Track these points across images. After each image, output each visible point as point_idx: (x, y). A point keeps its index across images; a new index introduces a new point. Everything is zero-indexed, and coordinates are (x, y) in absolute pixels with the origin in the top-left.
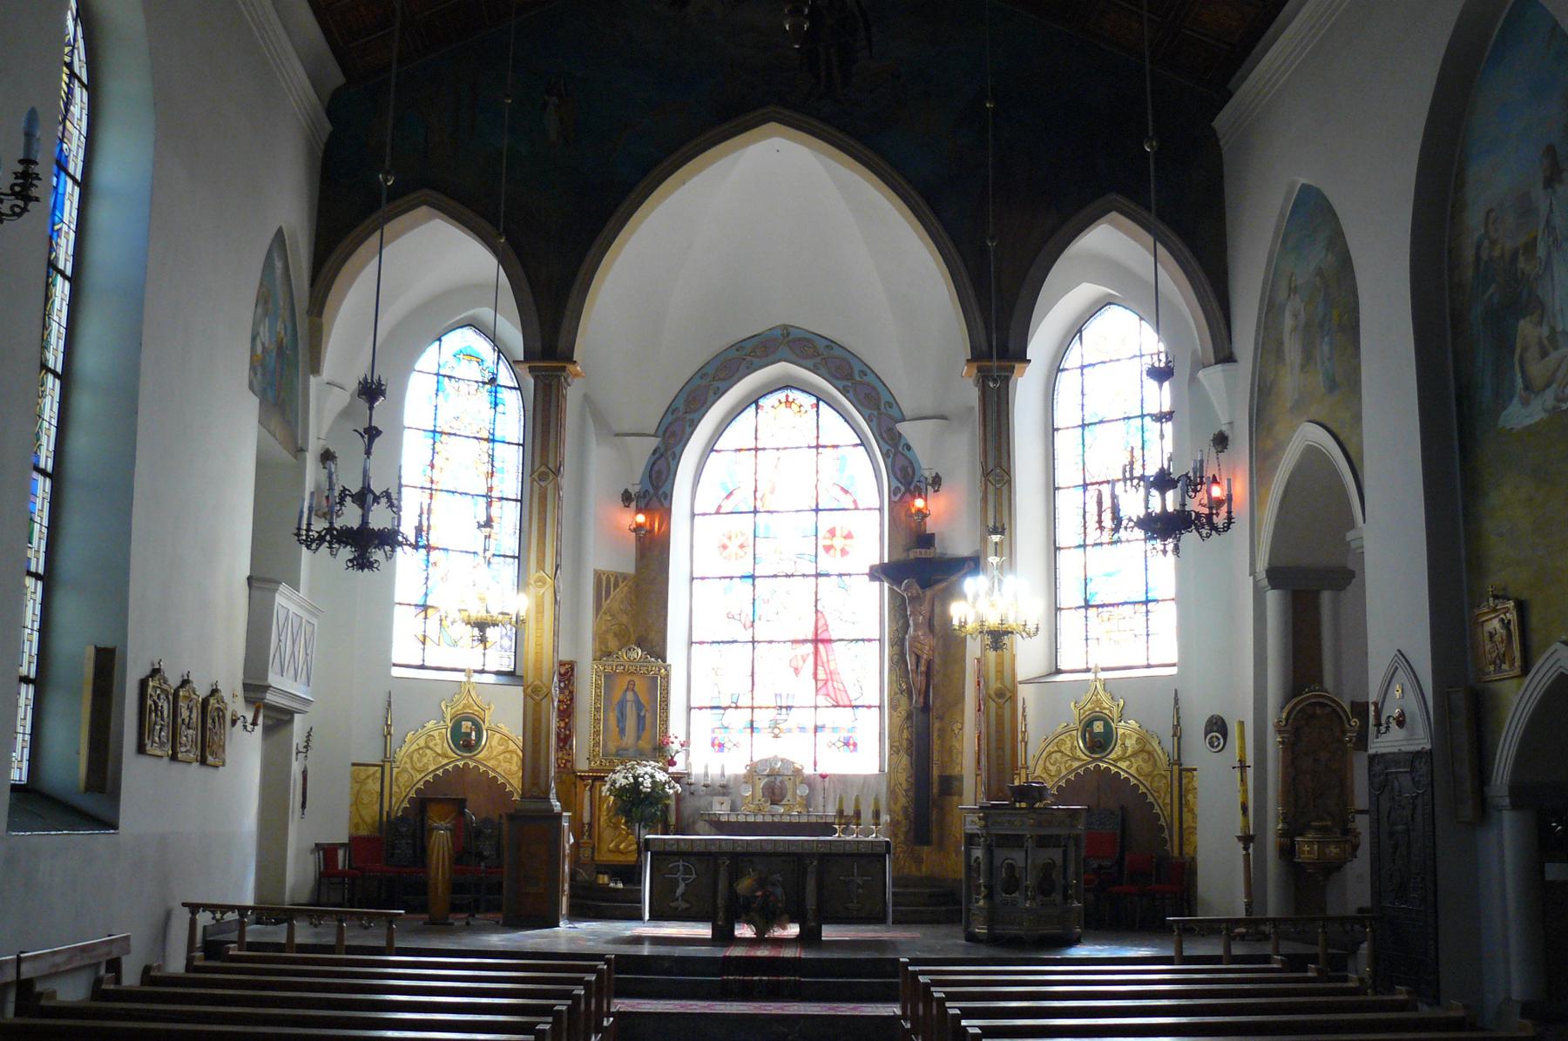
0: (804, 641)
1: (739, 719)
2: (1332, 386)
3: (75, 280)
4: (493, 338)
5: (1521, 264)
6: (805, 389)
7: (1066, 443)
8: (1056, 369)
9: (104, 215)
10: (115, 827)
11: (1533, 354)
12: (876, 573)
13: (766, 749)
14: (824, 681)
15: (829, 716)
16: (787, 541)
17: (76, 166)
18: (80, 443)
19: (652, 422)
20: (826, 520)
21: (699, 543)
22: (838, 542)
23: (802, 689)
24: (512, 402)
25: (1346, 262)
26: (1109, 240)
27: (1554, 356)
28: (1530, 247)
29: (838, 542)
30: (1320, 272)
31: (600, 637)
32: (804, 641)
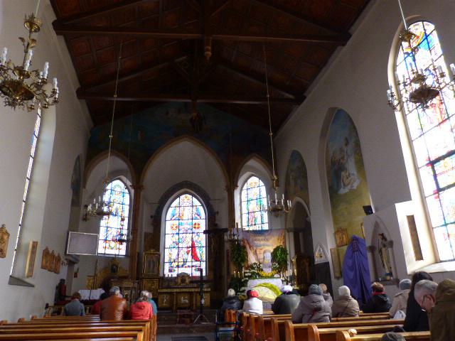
0: (441, 174)
1: (175, 264)
2: (302, 188)
3: (34, 158)
4: (125, 184)
5: (341, 161)
6: (190, 194)
7: (244, 205)
8: (241, 190)
9: (42, 146)
10: (413, 216)
11: (345, 179)
12: (205, 232)
13: (181, 270)
14: (195, 257)
15: (195, 263)
16: (186, 225)
17: (37, 134)
18: (33, 196)
19: (157, 201)
20: (194, 221)
21: (169, 226)
22: (197, 226)
23: (189, 257)
24: (127, 196)
25: (304, 165)
26: (252, 162)
27: (349, 179)
28: (343, 158)
29: (197, 226)
30: (298, 167)
31: (145, 247)
32: (441, 174)
